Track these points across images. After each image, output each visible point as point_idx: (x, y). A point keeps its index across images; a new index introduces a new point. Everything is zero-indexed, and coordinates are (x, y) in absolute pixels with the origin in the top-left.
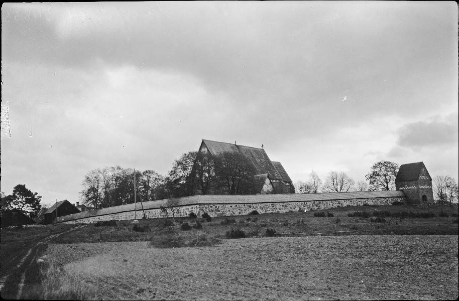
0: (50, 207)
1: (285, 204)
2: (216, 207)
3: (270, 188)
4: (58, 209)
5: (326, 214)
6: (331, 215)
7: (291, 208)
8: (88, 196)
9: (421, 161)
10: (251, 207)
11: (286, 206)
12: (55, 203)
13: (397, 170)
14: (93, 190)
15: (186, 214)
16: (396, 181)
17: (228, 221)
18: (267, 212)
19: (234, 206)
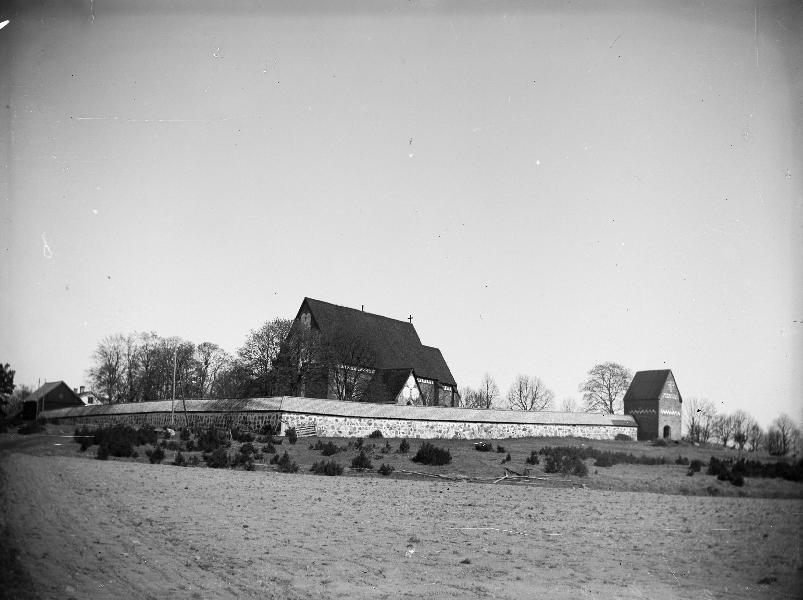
0: (34, 390)
1: (430, 424)
2: (311, 419)
3: (416, 394)
4: (47, 396)
5: (495, 447)
6: (501, 450)
7: (440, 431)
8: (99, 378)
9: (669, 368)
10: (370, 424)
11: (432, 427)
12: (41, 385)
13: (629, 381)
14: (110, 369)
15: (259, 426)
16: (626, 400)
17: (328, 447)
18: (398, 435)
19: (341, 420)
